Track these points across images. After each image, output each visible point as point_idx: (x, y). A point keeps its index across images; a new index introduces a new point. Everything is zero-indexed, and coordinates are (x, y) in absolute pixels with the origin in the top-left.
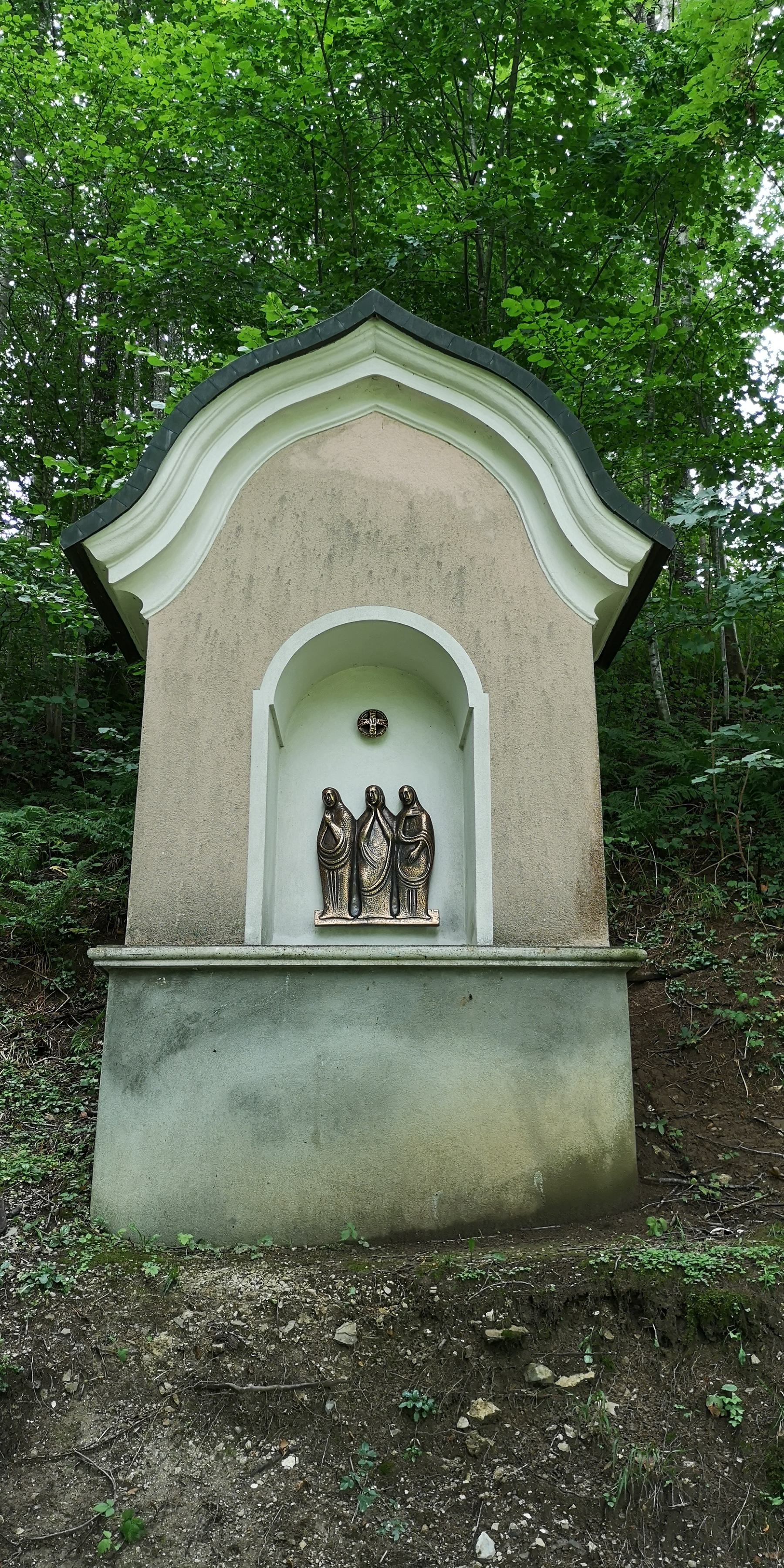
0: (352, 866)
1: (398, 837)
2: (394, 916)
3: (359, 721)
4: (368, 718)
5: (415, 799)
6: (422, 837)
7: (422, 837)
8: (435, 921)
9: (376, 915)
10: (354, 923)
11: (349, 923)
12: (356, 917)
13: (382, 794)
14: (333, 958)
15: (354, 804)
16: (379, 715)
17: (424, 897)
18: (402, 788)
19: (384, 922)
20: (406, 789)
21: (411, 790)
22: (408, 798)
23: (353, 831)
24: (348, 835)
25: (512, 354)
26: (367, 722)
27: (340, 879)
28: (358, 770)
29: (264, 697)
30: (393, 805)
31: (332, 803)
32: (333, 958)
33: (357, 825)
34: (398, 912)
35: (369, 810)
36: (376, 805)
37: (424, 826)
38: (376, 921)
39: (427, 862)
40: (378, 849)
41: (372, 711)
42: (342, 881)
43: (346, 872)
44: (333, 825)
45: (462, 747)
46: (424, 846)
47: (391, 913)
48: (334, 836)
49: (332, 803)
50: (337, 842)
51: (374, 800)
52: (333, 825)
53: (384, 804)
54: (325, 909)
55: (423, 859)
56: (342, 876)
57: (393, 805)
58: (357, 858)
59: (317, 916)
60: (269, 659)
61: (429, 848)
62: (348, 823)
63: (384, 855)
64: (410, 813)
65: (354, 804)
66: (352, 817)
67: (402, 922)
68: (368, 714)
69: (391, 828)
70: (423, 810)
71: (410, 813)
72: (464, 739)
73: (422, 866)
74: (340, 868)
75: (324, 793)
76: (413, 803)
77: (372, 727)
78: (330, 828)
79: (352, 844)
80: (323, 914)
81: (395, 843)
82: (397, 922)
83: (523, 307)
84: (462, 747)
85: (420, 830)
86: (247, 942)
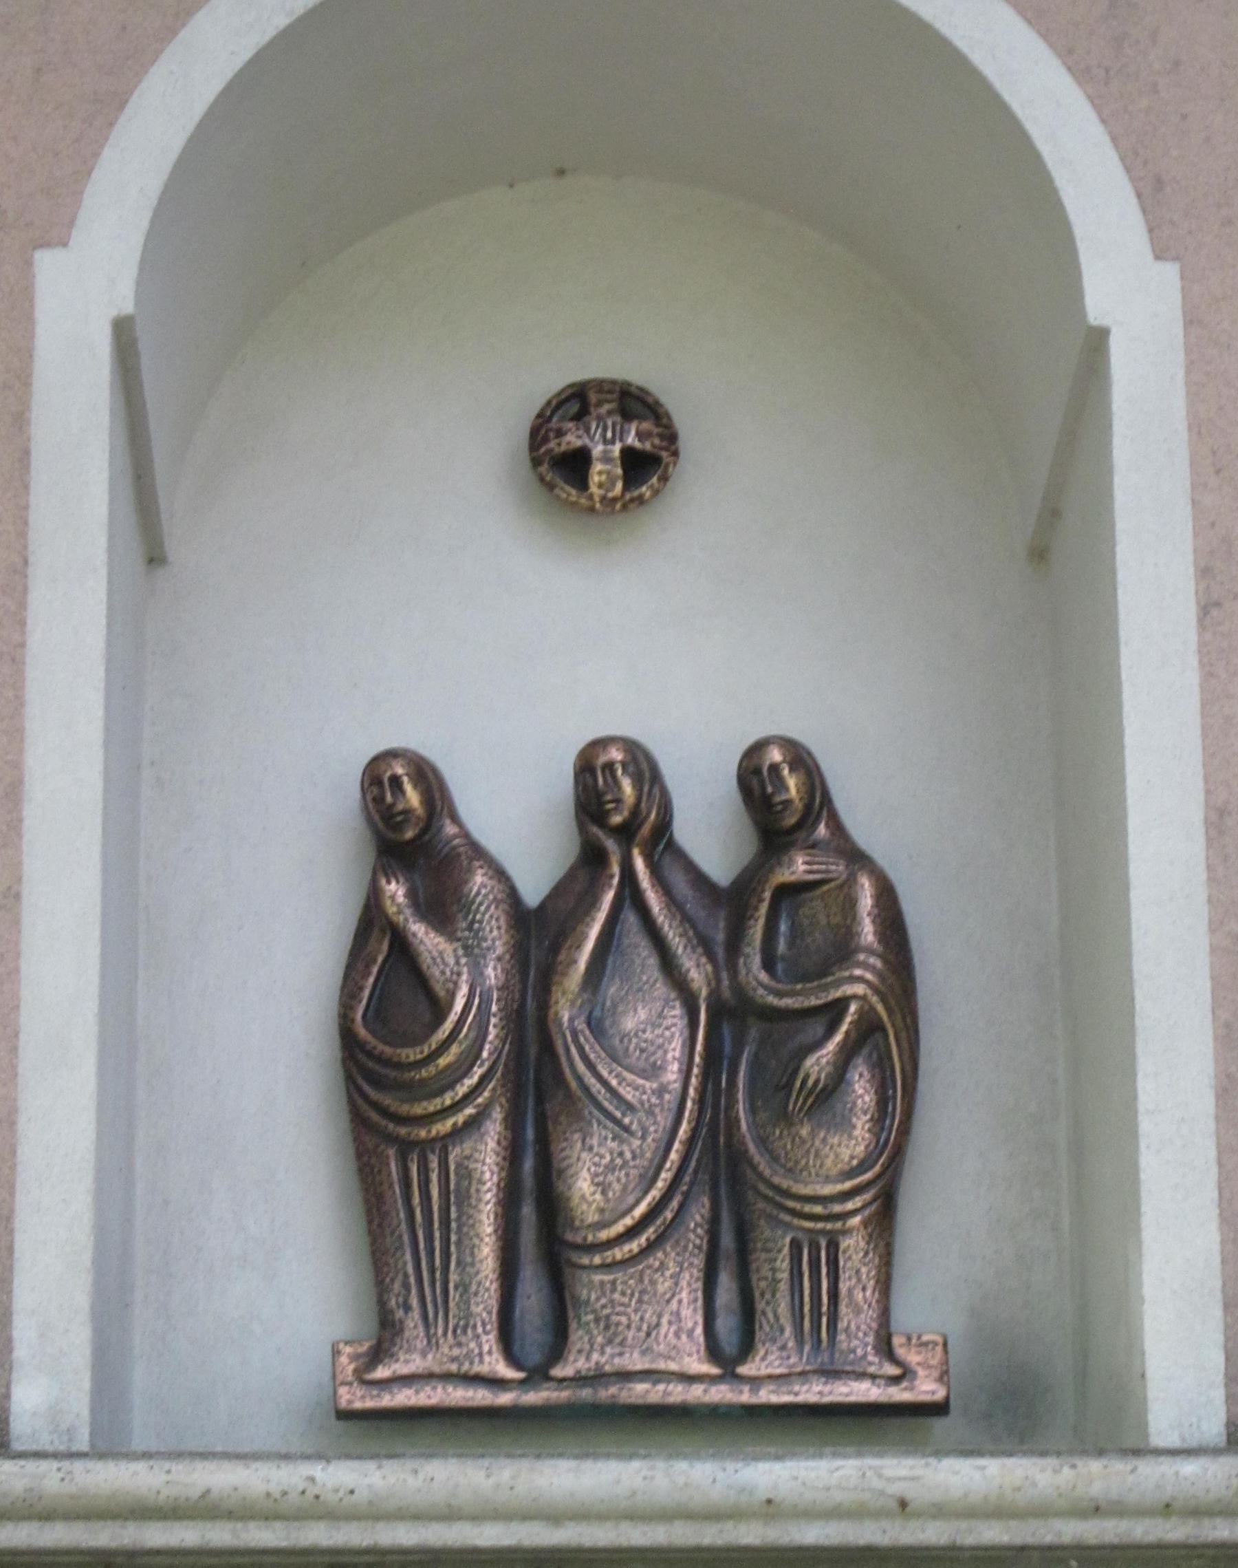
0: (514, 1123)
1: (739, 991)
2: (727, 1358)
3: (540, 432)
4: (581, 416)
5: (818, 801)
6: (858, 985)
7: (858, 985)
8: (927, 1389)
9: (635, 1361)
10: (532, 1397)
11: (505, 1398)
12: (538, 1375)
13: (656, 776)
14: (450, 1515)
15: (517, 825)
16: (633, 402)
17: (868, 1273)
18: (758, 747)
19: (677, 1393)
20: (775, 755)
21: (800, 758)
22: (782, 799)
23: (520, 955)
24: (492, 974)
25: (700, 1176)
26: (573, 440)
27: (458, 1195)
28: (546, 674)
29: (86, 284)
30: (710, 833)
31: (408, 827)
32: (450, 1515)
33: (540, 933)
34: (747, 1348)
35: (591, 859)
36: (626, 833)
37: (868, 932)
38: (641, 1392)
39: (883, 1102)
40: (647, 1044)
41: (600, 385)
42: (465, 1198)
43: (486, 1157)
44: (418, 930)
45: (1039, 554)
46: (869, 1029)
47: (713, 1351)
48: (421, 980)
49: (408, 827)
50: (439, 1010)
51: (613, 802)
52: (418, 930)
53: (664, 826)
54: (384, 1338)
55: (861, 1088)
56: (466, 1174)
57: (710, 833)
58: (540, 1090)
59: (348, 1367)
60: (109, 105)
61: (891, 1039)
62: (495, 934)
63: (672, 1074)
64: (798, 867)
65: (517, 825)
66: (513, 895)
67: (768, 1396)
68: (577, 401)
69: (704, 944)
70: (857, 858)
71: (798, 867)
72: (1051, 514)
73: (861, 1127)
74: (457, 1134)
75: (378, 779)
76: (808, 818)
77: (598, 454)
78: (402, 946)
79: (515, 1020)
80: (378, 1354)
81: (728, 1024)
82: (745, 1396)
83: (658, 1227)
84: (1039, 554)
85: (843, 950)
86: (17, 1446)
